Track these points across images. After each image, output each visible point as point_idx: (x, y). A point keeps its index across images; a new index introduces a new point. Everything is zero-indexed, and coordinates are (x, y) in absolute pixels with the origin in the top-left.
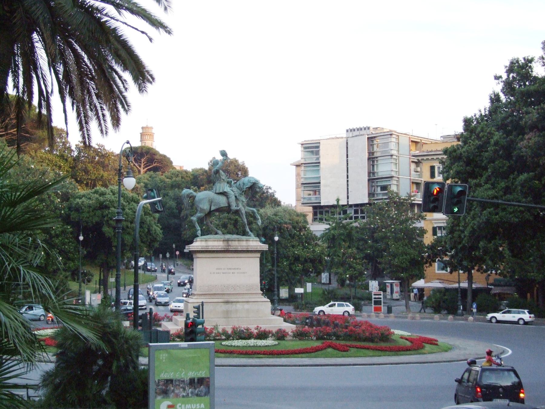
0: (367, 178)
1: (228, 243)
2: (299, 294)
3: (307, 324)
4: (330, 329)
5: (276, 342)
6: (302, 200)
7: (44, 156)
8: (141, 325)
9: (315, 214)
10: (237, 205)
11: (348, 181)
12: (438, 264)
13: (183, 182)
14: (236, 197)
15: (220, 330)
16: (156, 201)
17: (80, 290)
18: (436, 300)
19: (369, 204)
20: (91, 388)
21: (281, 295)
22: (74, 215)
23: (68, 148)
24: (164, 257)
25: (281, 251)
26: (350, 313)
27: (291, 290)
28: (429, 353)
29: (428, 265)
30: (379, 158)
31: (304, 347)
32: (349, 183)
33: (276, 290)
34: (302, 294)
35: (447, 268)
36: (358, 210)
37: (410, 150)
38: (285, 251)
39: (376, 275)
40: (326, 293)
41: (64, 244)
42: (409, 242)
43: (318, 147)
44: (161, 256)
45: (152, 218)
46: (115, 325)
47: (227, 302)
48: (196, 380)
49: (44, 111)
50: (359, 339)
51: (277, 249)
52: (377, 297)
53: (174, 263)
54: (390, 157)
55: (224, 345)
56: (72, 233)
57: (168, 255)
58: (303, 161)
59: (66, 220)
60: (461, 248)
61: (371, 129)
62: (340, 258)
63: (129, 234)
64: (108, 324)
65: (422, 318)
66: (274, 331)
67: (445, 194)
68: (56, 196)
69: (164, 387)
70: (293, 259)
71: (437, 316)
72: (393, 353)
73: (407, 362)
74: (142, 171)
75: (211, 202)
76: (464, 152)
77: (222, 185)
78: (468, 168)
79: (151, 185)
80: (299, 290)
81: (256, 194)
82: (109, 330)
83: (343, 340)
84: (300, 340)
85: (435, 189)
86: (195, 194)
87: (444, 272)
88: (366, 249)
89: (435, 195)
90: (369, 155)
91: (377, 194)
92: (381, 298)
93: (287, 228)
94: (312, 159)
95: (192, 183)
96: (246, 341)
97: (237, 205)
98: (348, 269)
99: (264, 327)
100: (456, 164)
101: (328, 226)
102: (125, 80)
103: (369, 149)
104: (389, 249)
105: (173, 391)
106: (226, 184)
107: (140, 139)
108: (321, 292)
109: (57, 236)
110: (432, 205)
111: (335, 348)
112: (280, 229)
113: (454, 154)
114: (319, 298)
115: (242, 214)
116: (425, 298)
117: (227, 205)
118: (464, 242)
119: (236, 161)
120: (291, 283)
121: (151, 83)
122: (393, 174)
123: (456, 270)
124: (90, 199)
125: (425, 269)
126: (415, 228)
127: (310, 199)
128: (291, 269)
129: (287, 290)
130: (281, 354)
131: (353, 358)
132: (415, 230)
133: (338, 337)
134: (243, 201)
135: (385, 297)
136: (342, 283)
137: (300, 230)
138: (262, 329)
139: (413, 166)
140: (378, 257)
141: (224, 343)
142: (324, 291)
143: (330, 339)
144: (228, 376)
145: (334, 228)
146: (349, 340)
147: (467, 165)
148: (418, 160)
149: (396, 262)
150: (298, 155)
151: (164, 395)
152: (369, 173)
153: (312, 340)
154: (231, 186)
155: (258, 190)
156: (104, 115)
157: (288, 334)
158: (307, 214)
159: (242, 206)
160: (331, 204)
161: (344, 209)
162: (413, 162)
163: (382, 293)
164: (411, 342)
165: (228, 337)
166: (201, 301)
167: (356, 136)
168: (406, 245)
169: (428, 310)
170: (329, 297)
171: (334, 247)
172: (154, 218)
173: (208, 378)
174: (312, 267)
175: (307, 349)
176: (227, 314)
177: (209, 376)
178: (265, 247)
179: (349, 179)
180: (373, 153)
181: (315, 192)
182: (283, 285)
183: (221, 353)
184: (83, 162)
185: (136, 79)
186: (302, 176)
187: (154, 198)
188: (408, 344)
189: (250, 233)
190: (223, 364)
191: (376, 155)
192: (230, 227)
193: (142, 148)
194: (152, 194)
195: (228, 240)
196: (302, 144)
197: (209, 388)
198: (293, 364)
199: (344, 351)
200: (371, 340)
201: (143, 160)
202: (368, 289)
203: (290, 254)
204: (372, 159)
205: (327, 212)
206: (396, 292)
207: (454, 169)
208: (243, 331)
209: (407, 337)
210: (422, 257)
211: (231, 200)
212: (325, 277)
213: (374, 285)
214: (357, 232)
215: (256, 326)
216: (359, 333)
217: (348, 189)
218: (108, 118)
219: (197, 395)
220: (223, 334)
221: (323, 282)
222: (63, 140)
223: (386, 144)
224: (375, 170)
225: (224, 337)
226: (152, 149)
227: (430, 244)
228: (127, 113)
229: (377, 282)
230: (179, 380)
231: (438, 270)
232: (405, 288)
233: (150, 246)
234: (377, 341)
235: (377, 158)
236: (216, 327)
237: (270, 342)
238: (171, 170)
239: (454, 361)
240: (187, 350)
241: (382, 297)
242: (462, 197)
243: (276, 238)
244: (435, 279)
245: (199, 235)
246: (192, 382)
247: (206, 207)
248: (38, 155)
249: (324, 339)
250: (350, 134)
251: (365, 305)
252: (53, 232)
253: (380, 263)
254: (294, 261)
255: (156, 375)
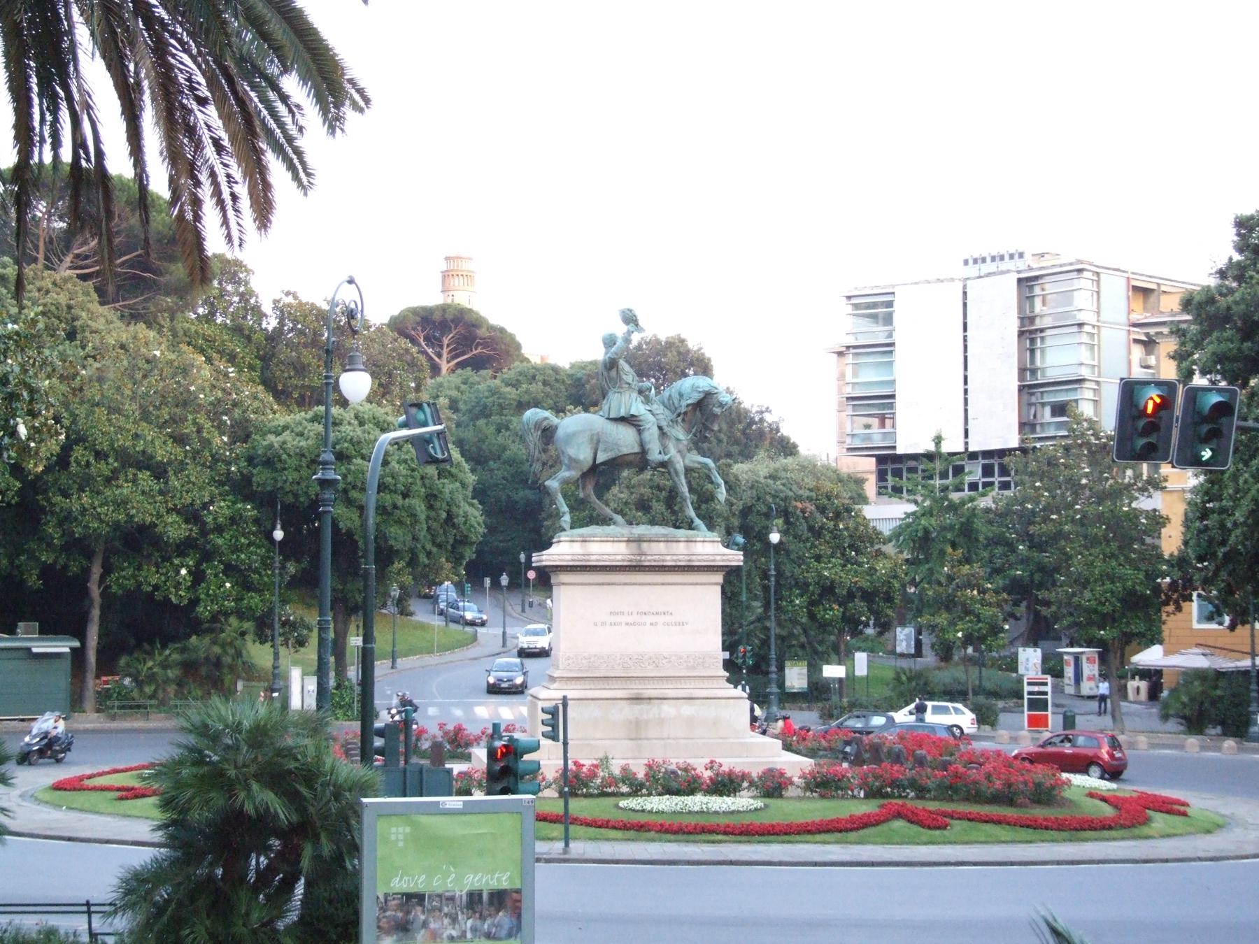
0: (1014, 384)
1: (639, 547)
2: (834, 679)
3: (845, 757)
4: (907, 772)
5: (759, 803)
6: (848, 440)
7: (193, 328)
8: (380, 752)
9: (881, 476)
10: (664, 450)
11: (966, 391)
12: (1200, 606)
13: (547, 395)
14: (660, 428)
15: (617, 771)
16: (431, 433)
17: (275, 668)
18: (1192, 699)
19: (1023, 450)
20: (247, 914)
21: (788, 684)
22: (261, 477)
23: (252, 309)
24: (496, 584)
25: (788, 569)
26: (966, 731)
27: (814, 669)
28: (1163, 837)
29: (1171, 608)
30: (1048, 332)
31: (830, 815)
32: (969, 396)
33: (773, 669)
34: (840, 680)
35: (1220, 615)
36: (993, 465)
37: (1130, 311)
38: (797, 571)
39: (1038, 633)
40: (904, 678)
41: (237, 549)
42: (1120, 548)
43: (890, 304)
44: (488, 581)
45: (458, 484)
46: (311, 751)
47: (637, 699)
48: (485, 897)
49: (189, 216)
50: (976, 797)
51: (777, 564)
52: (1036, 689)
53: (523, 601)
54: (1075, 329)
55: (624, 809)
56: (256, 521)
57: (504, 580)
58: (851, 341)
59: (242, 488)
60: (1225, 554)
61: (1027, 256)
62: (941, 590)
63: (399, 522)
64: (290, 749)
65: (1153, 746)
66: (754, 775)
67: (1178, 411)
68: (218, 427)
69: (400, 915)
70: (818, 591)
71: (1193, 741)
72: (1065, 834)
73: (1144, 857)
74: (445, 367)
75: (597, 442)
76: (1237, 303)
77: (626, 396)
78: (1248, 344)
79: (465, 402)
80: (833, 671)
81: (718, 425)
82: (292, 765)
83: (935, 799)
84: (822, 796)
85: (1151, 399)
86: (554, 420)
87: (1214, 626)
88: (1011, 567)
89: (1149, 416)
90: (1022, 325)
91: (1042, 425)
92: (1046, 693)
93: (803, 511)
94: (877, 334)
95: (569, 397)
96: (682, 798)
97: (664, 450)
98: (961, 619)
99: (729, 763)
100: (1215, 334)
101: (912, 508)
102: (298, 106)
103: (1021, 309)
104: (1070, 566)
105: (425, 924)
106: (635, 395)
107: (440, 288)
108: (890, 675)
109: (219, 529)
110: (1141, 442)
111: (913, 818)
112: (786, 514)
113: (1211, 309)
114: (887, 692)
115: (677, 473)
116: (1165, 694)
117: (637, 449)
118: (1233, 538)
119: (683, 341)
120: (816, 652)
121: (361, 110)
122: (1085, 372)
123: (1244, 623)
124: (302, 434)
125: (1164, 617)
126: (1136, 514)
127: (868, 438)
128: (812, 616)
129: (805, 671)
130: (769, 834)
131: (958, 847)
132: (1137, 517)
133: (922, 792)
134: (678, 440)
135: (1057, 689)
136: (945, 652)
137: (838, 516)
138: (725, 768)
139: (1138, 352)
140: (1040, 586)
141: (623, 803)
142: (898, 674)
143: (900, 797)
144: (572, 889)
145: (928, 513)
146: (951, 800)
147: (1243, 340)
148: (1147, 335)
149: (1087, 598)
150: (847, 327)
151: (401, 934)
152: (1022, 371)
153: (854, 797)
154: (647, 400)
155: (717, 410)
156: (234, 197)
157: (792, 783)
158: (865, 476)
159: (679, 453)
160: (921, 451)
161: (955, 465)
162: (1136, 341)
163: (1049, 679)
164: (1116, 807)
165: (637, 789)
166: (560, 694)
167: (988, 275)
168: (1113, 556)
169: (1172, 725)
170: (915, 689)
171: (927, 560)
172: (463, 485)
173: (518, 891)
174: (875, 606)
175: (838, 821)
176: (636, 731)
177: (519, 886)
178: (735, 558)
179: (969, 386)
180: (1032, 320)
181: (882, 419)
182: (796, 658)
183: (614, 828)
184: (289, 344)
185: (320, 100)
186: (849, 378)
187: (425, 424)
188: (1108, 811)
189: (698, 521)
190: (617, 857)
191: (1039, 324)
192: (658, 507)
193: (444, 308)
194: (421, 416)
195: (639, 540)
196: (849, 298)
197: (519, 917)
198: (796, 860)
199: (939, 828)
200: (1010, 801)
201: (446, 341)
202: (1017, 671)
203: (811, 577)
204: (1029, 334)
205: (912, 470)
206: (1090, 679)
207: (1210, 348)
208: (674, 772)
209: (1104, 794)
210: (1157, 589)
211: (646, 436)
212: (904, 637)
213: (1030, 659)
214: (990, 522)
215: (708, 761)
216: (975, 782)
217: (966, 411)
218: (245, 203)
219: (488, 936)
220: (624, 782)
221: (899, 650)
222: (242, 289)
223: (1067, 295)
224: (1038, 363)
225: (625, 789)
226: (471, 310)
227: (1176, 553)
228: (306, 194)
229: (1039, 651)
230: (440, 896)
231: (1199, 622)
232: (1113, 662)
233: (456, 559)
234: (1017, 800)
235: (1042, 330)
236: (605, 761)
237: (743, 801)
238: (517, 363)
239: (1228, 858)
240: (463, 818)
241: (1048, 689)
242: (1224, 420)
243: (775, 537)
244: (1190, 644)
245: (567, 526)
246: (474, 899)
247: (583, 453)
248: (179, 326)
249: (886, 796)
250: (973, 270)
251: (1004, 710)
252: (209, 519)
253: (1047, 604)
254: (821, 595)
255: (379, 885)
